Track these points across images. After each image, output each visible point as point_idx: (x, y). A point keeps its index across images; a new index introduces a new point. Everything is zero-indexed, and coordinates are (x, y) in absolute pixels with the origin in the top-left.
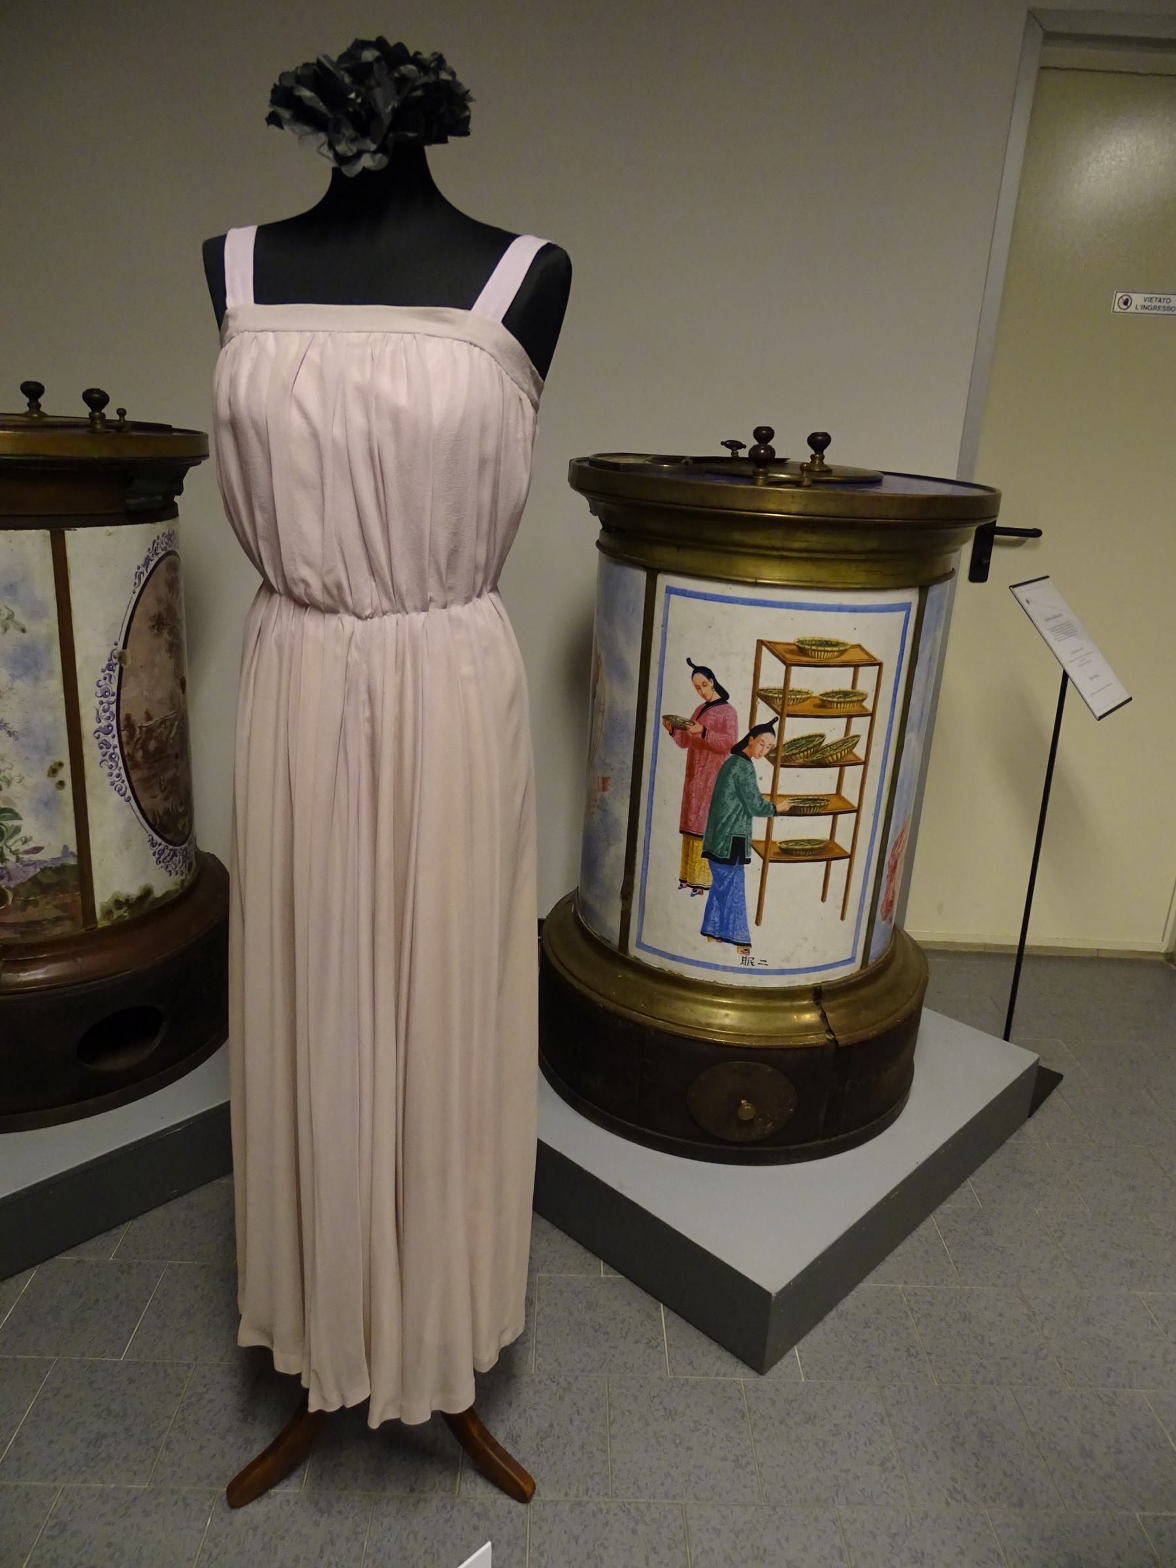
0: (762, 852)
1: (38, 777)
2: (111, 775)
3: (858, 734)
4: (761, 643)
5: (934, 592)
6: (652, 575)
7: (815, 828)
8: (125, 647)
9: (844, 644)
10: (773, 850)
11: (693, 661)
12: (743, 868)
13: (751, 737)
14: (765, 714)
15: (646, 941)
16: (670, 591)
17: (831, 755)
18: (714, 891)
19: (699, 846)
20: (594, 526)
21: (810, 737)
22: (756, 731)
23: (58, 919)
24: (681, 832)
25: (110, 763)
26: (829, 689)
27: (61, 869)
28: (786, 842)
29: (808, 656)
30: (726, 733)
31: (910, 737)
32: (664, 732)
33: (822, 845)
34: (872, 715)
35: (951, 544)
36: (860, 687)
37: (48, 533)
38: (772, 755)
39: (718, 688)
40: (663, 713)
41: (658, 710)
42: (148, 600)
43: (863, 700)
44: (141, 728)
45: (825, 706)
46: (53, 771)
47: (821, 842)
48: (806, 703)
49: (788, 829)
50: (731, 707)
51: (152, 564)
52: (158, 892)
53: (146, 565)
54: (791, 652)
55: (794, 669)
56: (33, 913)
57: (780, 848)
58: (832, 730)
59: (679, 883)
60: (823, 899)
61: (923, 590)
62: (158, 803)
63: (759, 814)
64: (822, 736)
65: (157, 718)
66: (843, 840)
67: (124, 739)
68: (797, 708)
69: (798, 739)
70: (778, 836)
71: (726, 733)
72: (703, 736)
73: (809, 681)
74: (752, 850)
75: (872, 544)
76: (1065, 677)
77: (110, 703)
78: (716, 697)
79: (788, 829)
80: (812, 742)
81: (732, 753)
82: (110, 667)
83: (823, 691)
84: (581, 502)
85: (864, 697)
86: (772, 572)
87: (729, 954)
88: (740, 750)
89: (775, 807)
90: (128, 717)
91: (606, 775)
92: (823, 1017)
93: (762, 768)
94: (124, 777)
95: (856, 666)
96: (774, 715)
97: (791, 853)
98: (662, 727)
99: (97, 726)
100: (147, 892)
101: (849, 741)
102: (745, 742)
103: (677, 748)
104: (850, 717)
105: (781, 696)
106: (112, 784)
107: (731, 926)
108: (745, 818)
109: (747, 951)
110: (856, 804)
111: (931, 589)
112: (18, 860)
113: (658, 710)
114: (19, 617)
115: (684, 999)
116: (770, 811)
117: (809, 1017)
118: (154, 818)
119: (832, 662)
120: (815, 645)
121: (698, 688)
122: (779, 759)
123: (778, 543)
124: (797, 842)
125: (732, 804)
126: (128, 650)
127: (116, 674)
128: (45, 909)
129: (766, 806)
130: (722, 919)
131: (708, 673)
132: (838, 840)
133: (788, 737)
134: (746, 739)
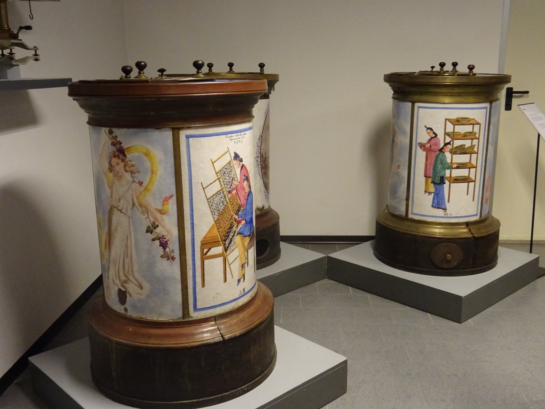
3: (475, 144)
4: (446, 119)
5: (494, 104)
6: (413, 103)
7: (463, 172)
8: (262, 133)
9: (469, 118)
10: (452, 179)
12: (443, 185)
13: (444, 147)
14: (448, 140)
15: (415, 212)
16: (419, 107)
17: (468, 151)
18: (435, 193)
19: (430, 180)
21: (461, 145)
22: (446, 144)
25: (258, 166)
26: (466, 132)
29: (460, 122)
30: (437, 146)
31: (490, 146)
32: (418, 148)
33: (466, 178)
34: (479, 139)
35: (499, 90)
36: (475, 131)
39: (434, 133)
40: (418, 142)
43: (476, 135)
45: (465, 136)
47: (466, 177)
49: (457, 173)
50: (438, 138)
54: (455, 121)
55: (456, 126)
57: (454, 179)
58: (467, 143)
59: (424, 192)
60: (467, 194)
61: (491, 103)
63: (448, 169)
64: (465, 145)
66: (472, 176)
68: (457, 137)
69: (458, 146)
70: (453, 175)
71: (437, 146)
73: (461, 129)
75: (476, 90)
76: (539, 135)
78: (434, 135)
79: (457, 173)
80: (462, 147)
81: (439, 151)
82: (259, 139)
83: (464, 132)
84: (387, 85)
85: (476, 134)
86: (447, 100)
87: (440, 212)
88: (441, 150)
89: (452, 166)
91: (398, 164)
92: (470, 230)
93: (448, 155)
94: (261, 171)
95: (473, 125)
97: (457, 180)
101: (472, 147)
102: (443, 148)
103: (423, 152)
104: (472, 139)
105: (452, 134)
106: (258, 173)
107: (440, 203)
109: (446, 211)
110: (475, 165)
111: (493, 103)
115: (427, 227)
116: (451, 168)
117: (465, 230)
119: (466, 124)
120: (461, 119)
121: (428, 134)
123: (450, 91)
124: (459, 177)
125: (439, 166)
126: (263, 135)
127: (260, 141)
129: (450, 166)
130: (438, 201)
131: (431, 129)
132: (471, 176)
133: (455, 146)
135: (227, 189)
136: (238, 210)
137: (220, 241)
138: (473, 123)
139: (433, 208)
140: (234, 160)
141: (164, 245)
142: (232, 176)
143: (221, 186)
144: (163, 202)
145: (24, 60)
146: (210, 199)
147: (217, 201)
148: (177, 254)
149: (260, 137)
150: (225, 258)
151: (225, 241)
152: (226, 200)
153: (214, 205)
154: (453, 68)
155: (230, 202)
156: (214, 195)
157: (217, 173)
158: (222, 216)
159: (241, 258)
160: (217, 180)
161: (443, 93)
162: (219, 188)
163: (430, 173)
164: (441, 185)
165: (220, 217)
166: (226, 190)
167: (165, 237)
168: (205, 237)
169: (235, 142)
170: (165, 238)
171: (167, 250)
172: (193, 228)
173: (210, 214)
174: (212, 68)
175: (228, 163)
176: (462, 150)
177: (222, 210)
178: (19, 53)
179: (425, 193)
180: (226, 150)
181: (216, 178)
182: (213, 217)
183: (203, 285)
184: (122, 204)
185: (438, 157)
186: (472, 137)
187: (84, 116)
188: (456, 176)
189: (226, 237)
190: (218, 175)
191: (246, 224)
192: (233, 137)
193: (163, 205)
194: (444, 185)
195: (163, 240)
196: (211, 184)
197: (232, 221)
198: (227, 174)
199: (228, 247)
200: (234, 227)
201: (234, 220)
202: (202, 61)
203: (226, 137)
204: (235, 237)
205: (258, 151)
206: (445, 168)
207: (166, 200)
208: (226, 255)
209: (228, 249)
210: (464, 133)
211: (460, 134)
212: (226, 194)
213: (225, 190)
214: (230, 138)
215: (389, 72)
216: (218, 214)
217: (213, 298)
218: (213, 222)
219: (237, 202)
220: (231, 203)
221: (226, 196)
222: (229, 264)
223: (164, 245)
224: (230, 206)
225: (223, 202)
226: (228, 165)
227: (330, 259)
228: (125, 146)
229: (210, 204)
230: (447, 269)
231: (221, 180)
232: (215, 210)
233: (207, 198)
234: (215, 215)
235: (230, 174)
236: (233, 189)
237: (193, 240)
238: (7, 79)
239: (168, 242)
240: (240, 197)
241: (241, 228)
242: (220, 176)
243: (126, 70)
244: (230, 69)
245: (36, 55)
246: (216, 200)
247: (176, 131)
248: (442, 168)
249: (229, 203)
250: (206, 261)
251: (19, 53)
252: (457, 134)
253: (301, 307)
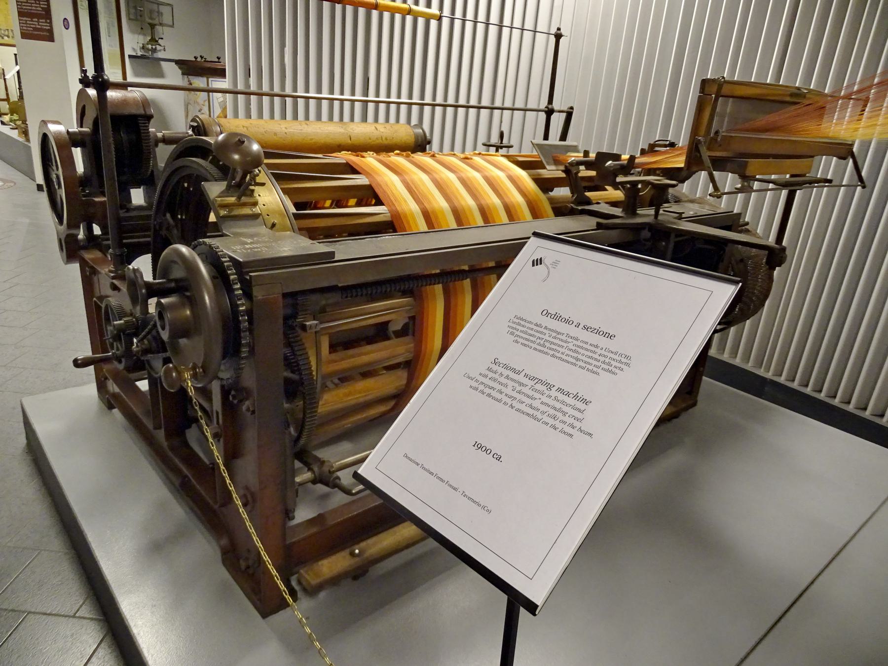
145: (160, 51)
178: (158, 47)
184: (191, 102)
187: (180, 72)
207: (205, 101)
228: (192, 82)
238: (412, 231)
243: (196, 58)
251: (158, 47)
253: (110, 354)
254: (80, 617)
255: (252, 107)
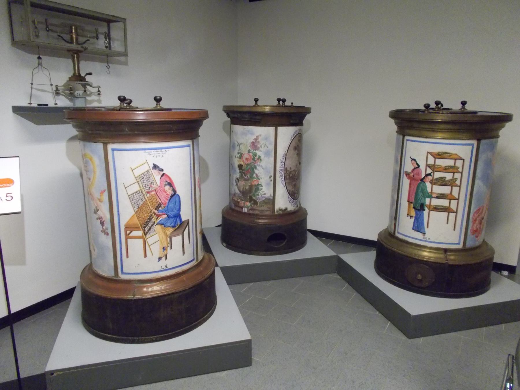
0: (429, 208)
1: (267, 178)
2: (281, 180)
4: (428, 153)
7: (445, 203)
8: (287, 152)
9: (451, 153)
11: (412, 158)
14: (429, 171)
15: (400, 231)
16: (408, 140)
17: (448, 183)
19: (412, 205)
20: (395, 128)
21: (442, 177)
22: (427, 175)
23: (267, 211)
24: (408, 201)
25: (281, 177)
27: (269, 199)
28: (436, 206)
32: (405, 176)
33: (447, 208)
36: (457, 165)
37: (274, 127)
38: (431, 182)
39: (417, 164)
40: (405, 171)
41: (403, 171)
42: (293, 143)
44: (289, 171)
45: (446, 169)
46: (270, 177)
47: (446, 207)
48: (440, 168)
49: (436, 202)
51: (295, 135)
52: (289, 209)
53: (294, 135)
54: (436, 155)
56: (262, 208)
57: (434, 207)
58: (448, 176)
60: (447, 223)
62: (291, 189)
63: (428, 197)
64: (445, 177)
65: (293, 169)
67: (285, 173)
68: (438, 169)
72: (414, 176)
73: (441, 162)
74: (426, 207)
77: (283, 164)
79: (436, 202)
80: (442, 179)
83: (445, 166)
84: (392, 121)
85: (458, 168)
87: (419, 235)
88: (422, 180)
90: (286, 168)
93: (428, 185)
94: (284, 181)
95: (455, 159)
96: (431, 171)
97: (437, 209)
98: (404, 175)
99: (280, 169)
100: (286, 209)
101: (454, 180)
102: (424, 178)
105: (433, 166)
106: (281, 182)
108: (424, 198)
112: (261, 196)
113: (403, 171)
114: (267, 145)
116: (430, 197)
118: (290, 192)
119: (447, 158)
121: (412, 164)
122: (433, 183)
124: (439, 206)
126: (288, 153)
127: (285, 158)
128: (265, 208)
130: (417, 225)
131: (415, 160)
133: (435, 177)
134: (424, 177)
135: (145, 190)
136: (158, 206)
137: (139, 227)
138: (456, 158)
139: (413, 230)
140: (153, 169)
141: (102, 223)
142: (151, 181)
143: (140, 188)
144: (101, 193)
146: (131, 196)
147: (137, 197)
148: (109, 231)
149: (285, 155)
150: (144, 241)
151: (145, 227)
152: (145, 198)
153: (134, 200)
154: (462, 107)
155: (149, 200)
156: (134, 193)
157: (136, 178)
158: (141, 209)
159: (162, 243)
160: (136, 182)
161: (426, 128)
162: (138, 189)
163: (413, 199)
164: (421, 211)
165: (140, 210)
166: (145, 191)
167: (102, 218)
168: (128, 222)
169: (154, 156)
170: (102, 219)
171: (104, 227)
172: (119, 214)
173: (131, 206)
174: (258, 102)
175: (147, 171)
176: (442, 182)
177: (142, 205)
179: (407, 216)
180: (145, 161)
181: (136, 181)
182: (134, 209)
183: (128, 257)
185: (420, 186)
186: (455, 171)
188: (436, 205)
189: (145, 225)
190: (137, 179)
191: (168, 218)
192: (151, 152)
193: (101, 196)
194: (424, 211)
195: (102, 220)
196: (131, 185)
197: (151, 214)
198: (146, 179)
199: (147, 233)
200: (153, 218)
201: (153, 213)
202: (159, 97)
203: (145, 152)
204: (154, 226)
205: (282, 166)
206: (425, 196)
207: (103, 192)
208: (146, 238)
209: (148, 234)
210: (445, 166)
211: (440, 167)
212: (145, 193)
213: (144, 191)
214: (148, 153)
215: (394, 109)
216: (138, 208)
217: (135, 267)
218: (134, 213)
219: (156, 200)
220: (150, 201)
221: (145, 195)
222: (149, 245)
223: (102, 223)
224: (148, 203)
225: (142, 199)
226: (147, 172)
227: (338, 257)
229: (131, 199)
230: (419, 287)
231: (140, 183)
232: (135, 204)
233: (128, 195)
234: (135, 207)
235: (148, 179)
236: (152, 191)
237: (119, 223)
239: (105, 222)
240: (160, 197)
241: (161, 220)
242: (139, 180)
244: (255, 103)
245: (99, 91)
246: (136, 197)
247: (105, 144)
248: (422, 196)
249: (148, 200)
250: (129, 240)
252: (438, 167)
254: (430, 207)
255: (467, 202)
